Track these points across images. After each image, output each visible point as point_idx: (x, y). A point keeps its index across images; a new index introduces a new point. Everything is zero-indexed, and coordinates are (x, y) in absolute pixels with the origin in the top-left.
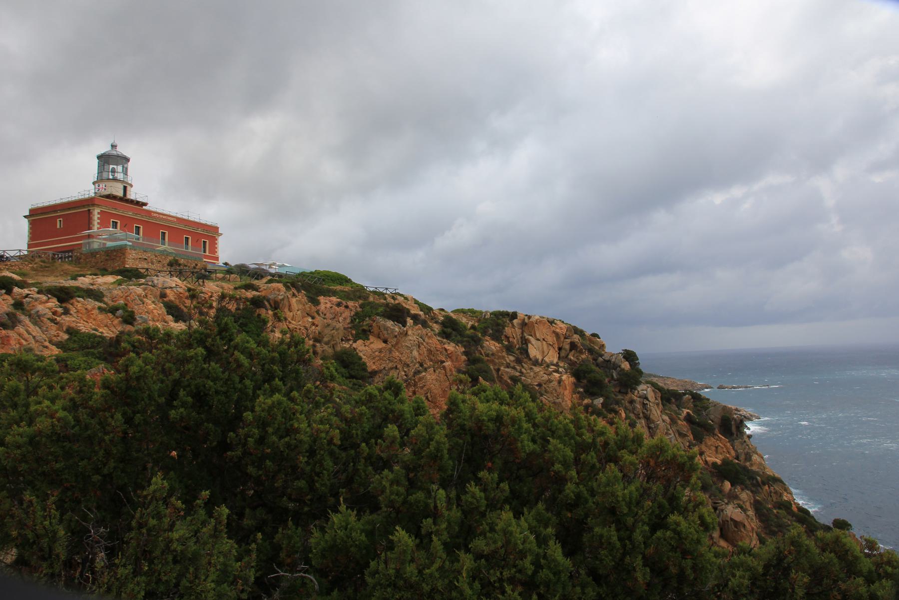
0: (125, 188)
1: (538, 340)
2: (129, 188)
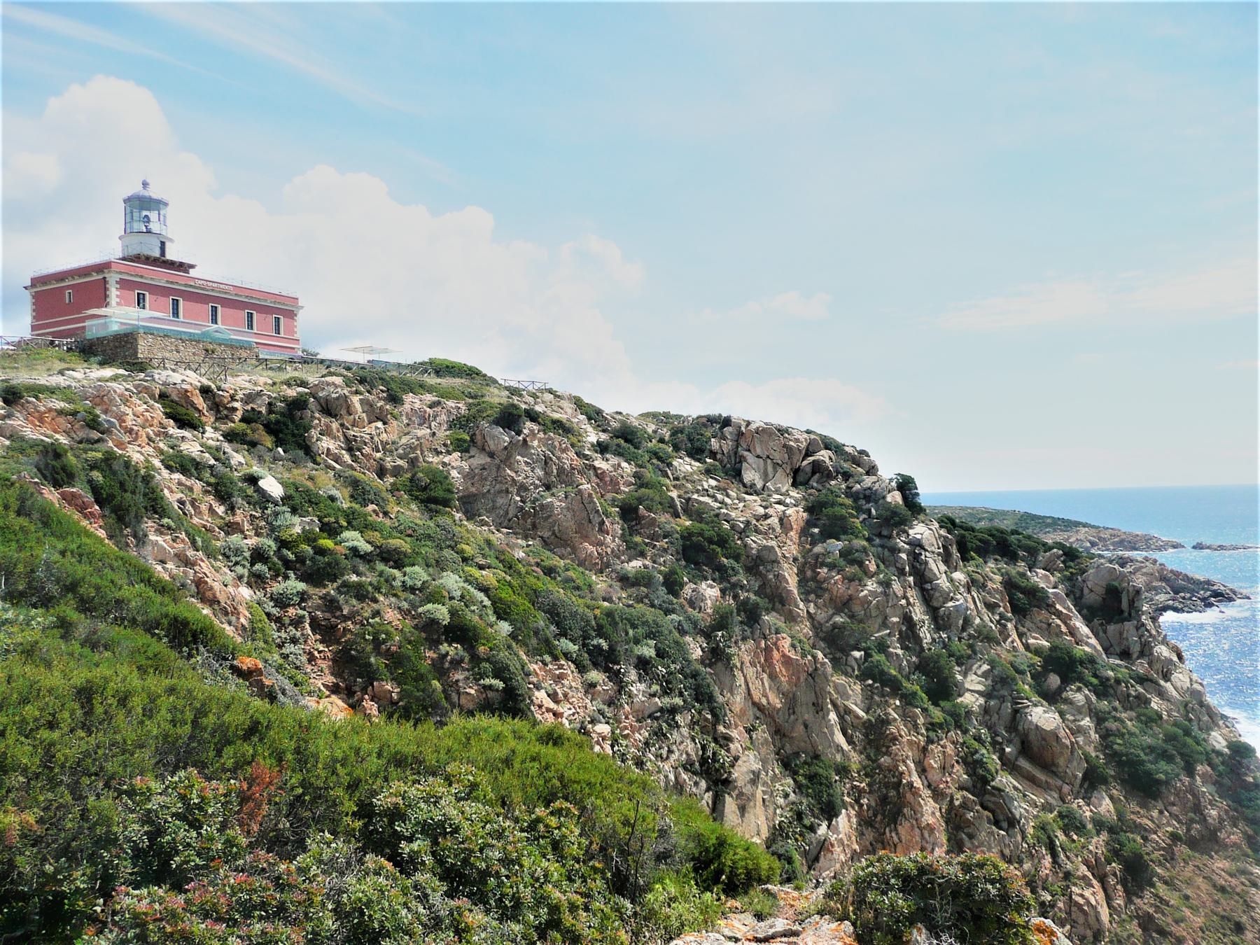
0: (163, 244)
1: (758, 457)
2: (168, 245)
